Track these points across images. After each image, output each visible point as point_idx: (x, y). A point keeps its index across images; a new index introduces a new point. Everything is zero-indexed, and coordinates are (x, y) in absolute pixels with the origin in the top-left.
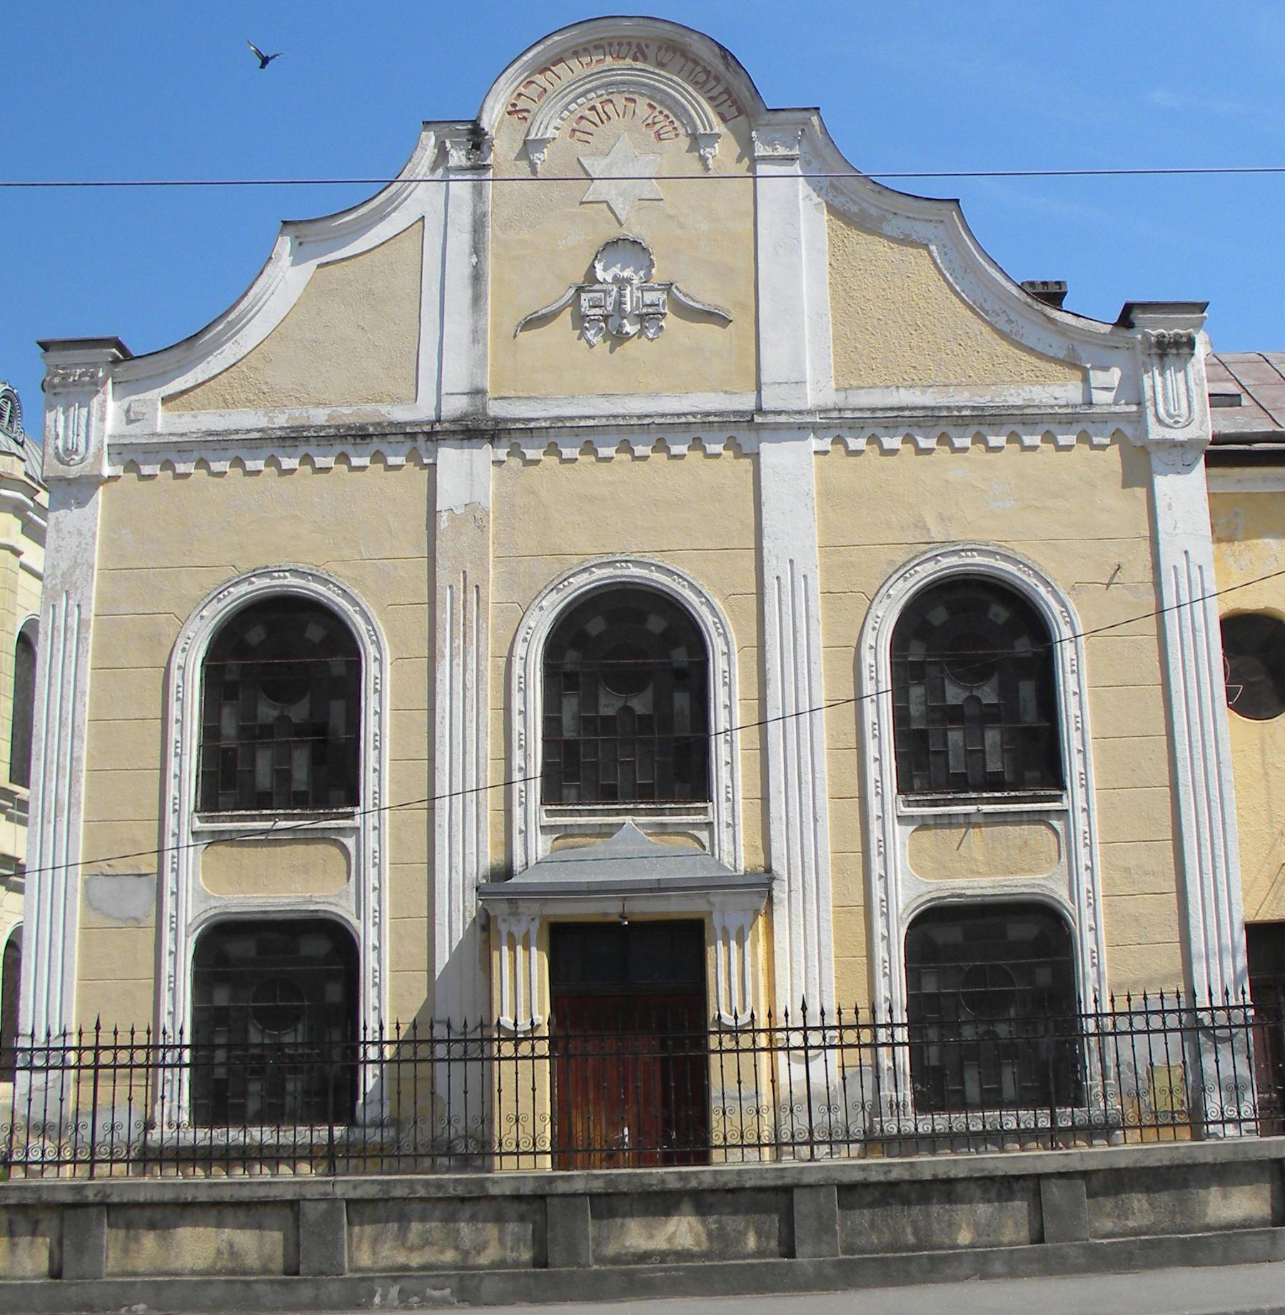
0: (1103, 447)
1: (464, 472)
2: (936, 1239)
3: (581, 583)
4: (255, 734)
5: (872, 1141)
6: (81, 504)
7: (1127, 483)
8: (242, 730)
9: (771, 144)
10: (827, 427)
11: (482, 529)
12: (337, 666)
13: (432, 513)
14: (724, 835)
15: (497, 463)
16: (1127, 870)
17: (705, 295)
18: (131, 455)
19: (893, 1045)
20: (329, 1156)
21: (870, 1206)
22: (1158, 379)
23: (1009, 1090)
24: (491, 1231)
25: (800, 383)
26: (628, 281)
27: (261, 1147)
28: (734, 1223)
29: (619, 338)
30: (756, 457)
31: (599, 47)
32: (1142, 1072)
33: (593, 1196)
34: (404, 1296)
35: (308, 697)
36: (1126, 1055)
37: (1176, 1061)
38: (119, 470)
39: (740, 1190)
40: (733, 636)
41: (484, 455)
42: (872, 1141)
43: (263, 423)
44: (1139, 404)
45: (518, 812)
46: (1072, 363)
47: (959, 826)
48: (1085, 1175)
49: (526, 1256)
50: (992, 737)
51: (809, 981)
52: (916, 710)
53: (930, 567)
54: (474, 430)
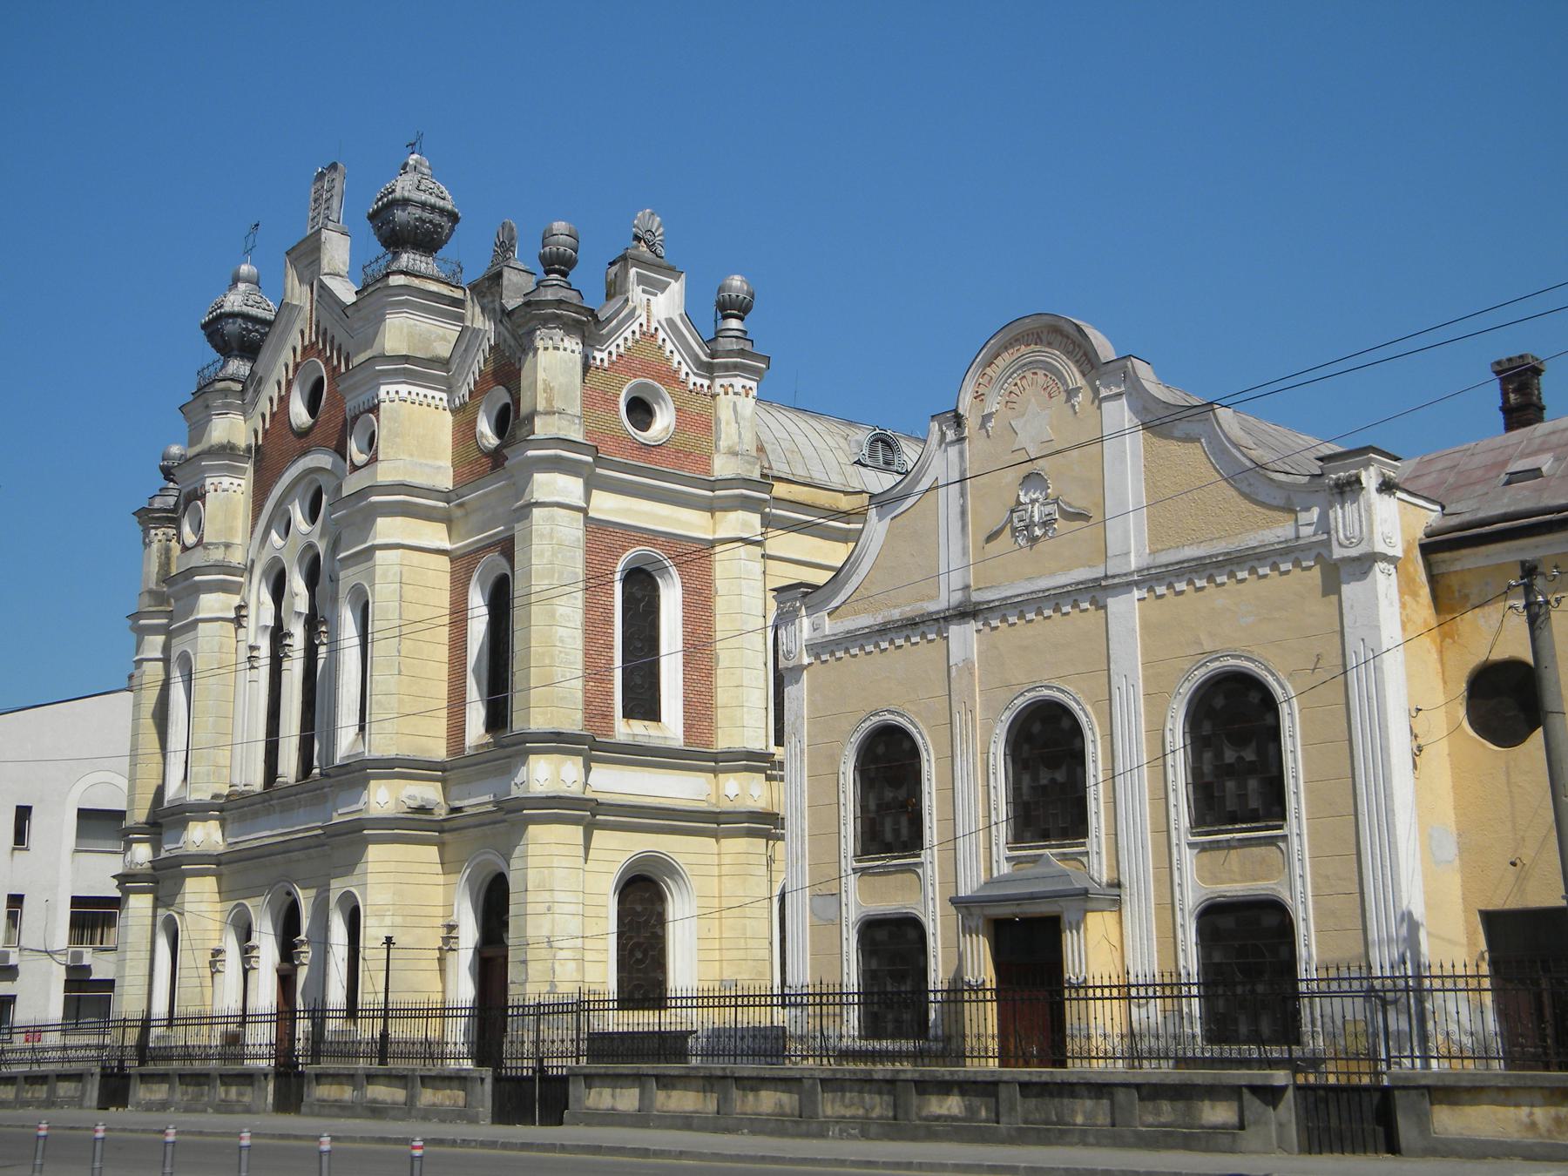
0: (1309, 568)
1: (964, 639)
2: (1067, 1119)
3: (1020, 703)
4: (883, 807)
5: (1181, 1062)
6: (797, 682)
7: (1326, 593)
8: (879, 806)
9: (1107, 387)
10: (1143, 581)
11: (972, 674)
12: (1207, 728)
13: (949, 667)
14: (1094, 859)
15: (978, 631)
16: (1327, 877)
17: (1078, 501)
18: (815, 649)
19: (1190, 997)
20: (917, 1056)
21: (1036, 1096)
22: (1340, 512)
23: (1266, 1028)
24: (877, 1098)
25: (1127, 554)
26: (1037, 500)
27: (887, 1051)
28: (977, 1101)
29: (1034, 540)
30: (1105, 607)
31: (1016, 341)
32: (1339, 1022)
33: (916, 1082)
34: (841, 1131)
35: (1254, 744)
36: (1328, 1010)
37: (1360, 1017)
38: (812, 660)
39: (975, 1082)
40: (1097, 729)
41: (973, 626)
42: (1181, 1062)
43: (871, 622)
44: (1329, 533)
45: (994, 848)
46: (1289, 509)
47: (1223, 848)
48: (1138, 1087)
49: (891, 1114)
50: (1253, 784)
51: (1130, 952)
52: (1207, 768)
53: (1203, 670)
54: (966, 612)
